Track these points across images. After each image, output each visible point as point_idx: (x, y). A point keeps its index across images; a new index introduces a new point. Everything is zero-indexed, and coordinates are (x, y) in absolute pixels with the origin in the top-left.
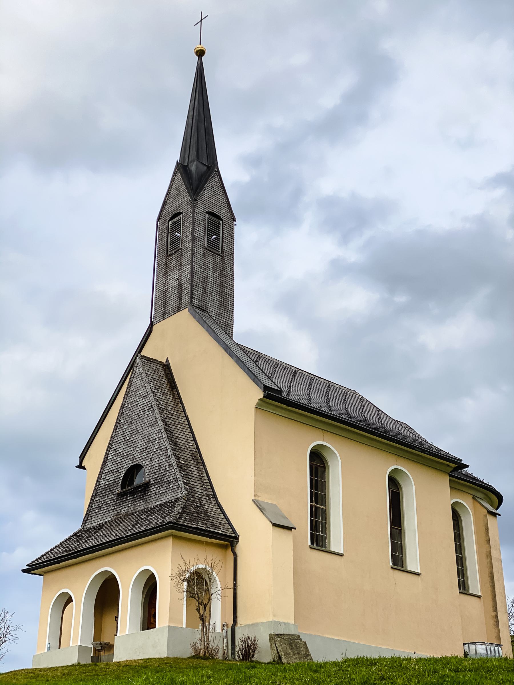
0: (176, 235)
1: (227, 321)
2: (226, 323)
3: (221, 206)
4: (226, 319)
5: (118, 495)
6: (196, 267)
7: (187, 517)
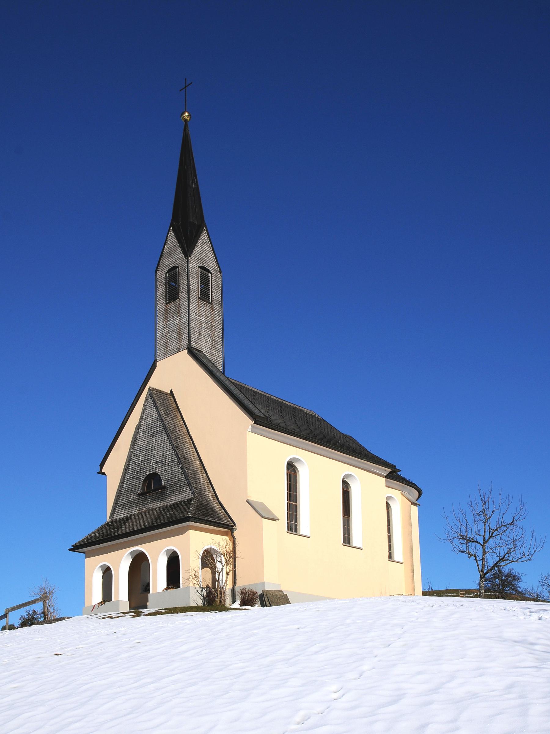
0: (173, 285)
1: (217, 359)
2: (217, 360)
3: (210, 261)
4: (216, 357)
5: (139, 495)
6: (192, 315)
7: (200, 513)
